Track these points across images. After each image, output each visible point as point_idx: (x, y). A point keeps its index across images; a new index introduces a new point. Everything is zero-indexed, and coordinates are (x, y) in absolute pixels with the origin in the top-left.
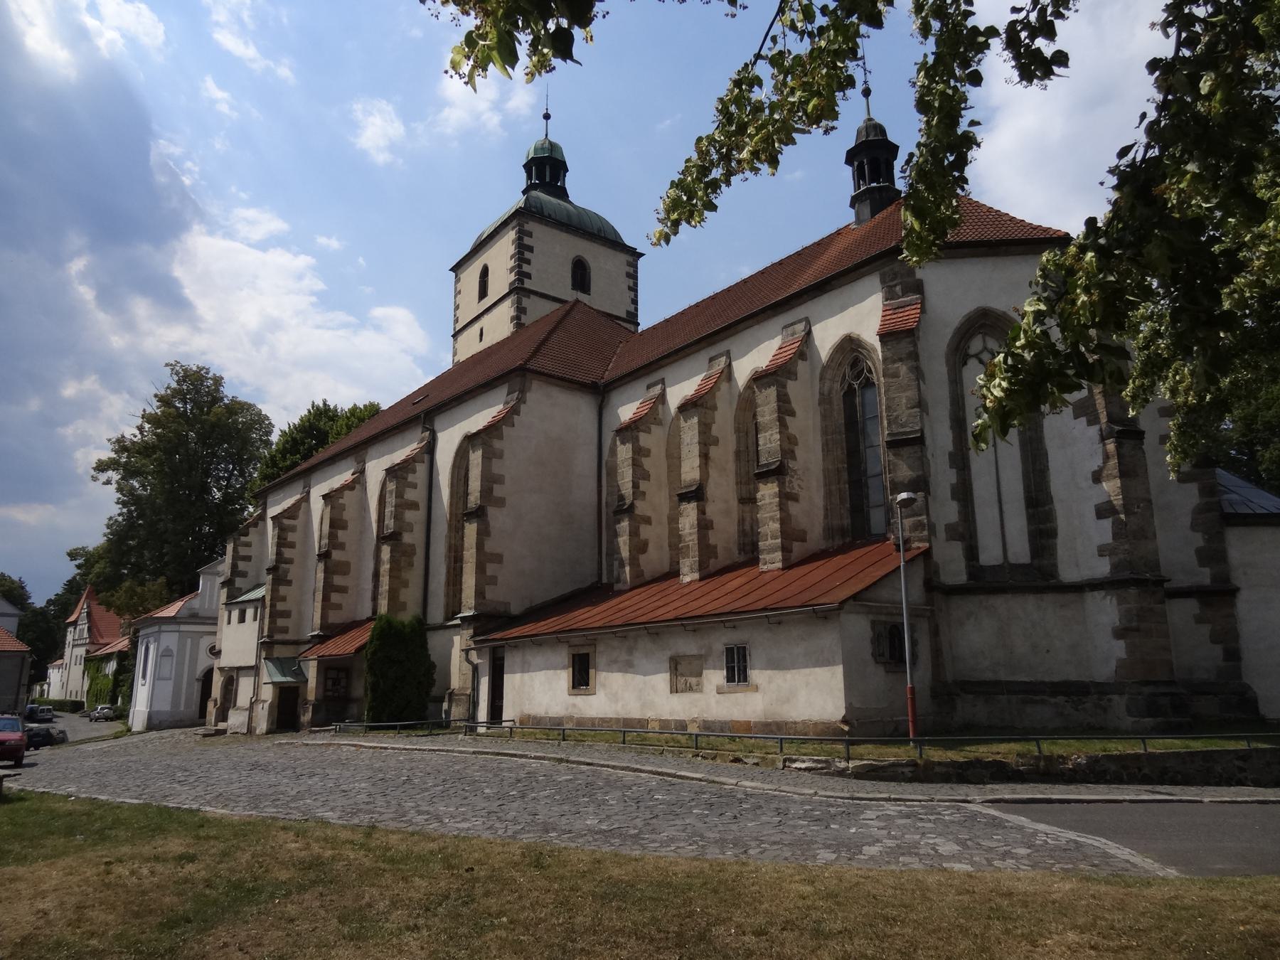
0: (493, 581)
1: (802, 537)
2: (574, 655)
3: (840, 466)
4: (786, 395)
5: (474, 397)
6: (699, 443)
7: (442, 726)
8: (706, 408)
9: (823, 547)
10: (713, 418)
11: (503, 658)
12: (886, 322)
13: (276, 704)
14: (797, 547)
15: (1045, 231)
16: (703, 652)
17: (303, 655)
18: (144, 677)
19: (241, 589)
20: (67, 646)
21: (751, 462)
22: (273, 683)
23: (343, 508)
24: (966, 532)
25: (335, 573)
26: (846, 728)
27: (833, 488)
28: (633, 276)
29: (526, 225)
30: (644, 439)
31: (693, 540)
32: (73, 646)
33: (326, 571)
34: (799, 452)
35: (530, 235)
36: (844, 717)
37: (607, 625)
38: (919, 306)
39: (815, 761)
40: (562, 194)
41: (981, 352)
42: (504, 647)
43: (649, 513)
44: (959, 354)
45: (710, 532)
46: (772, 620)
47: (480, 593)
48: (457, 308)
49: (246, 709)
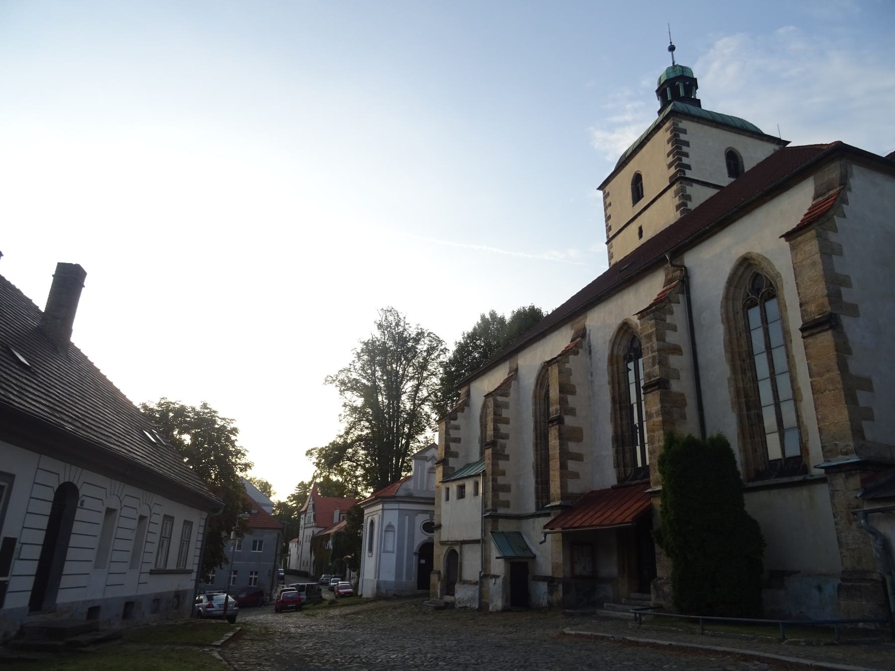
18: (371, 550)
19: (454, 468)
20: (300, 529)
23: (569, 373)
32: (304, 528)
33: (561, 437)
35: (684, 131)
40: (698, 103)
49: (476, 583)
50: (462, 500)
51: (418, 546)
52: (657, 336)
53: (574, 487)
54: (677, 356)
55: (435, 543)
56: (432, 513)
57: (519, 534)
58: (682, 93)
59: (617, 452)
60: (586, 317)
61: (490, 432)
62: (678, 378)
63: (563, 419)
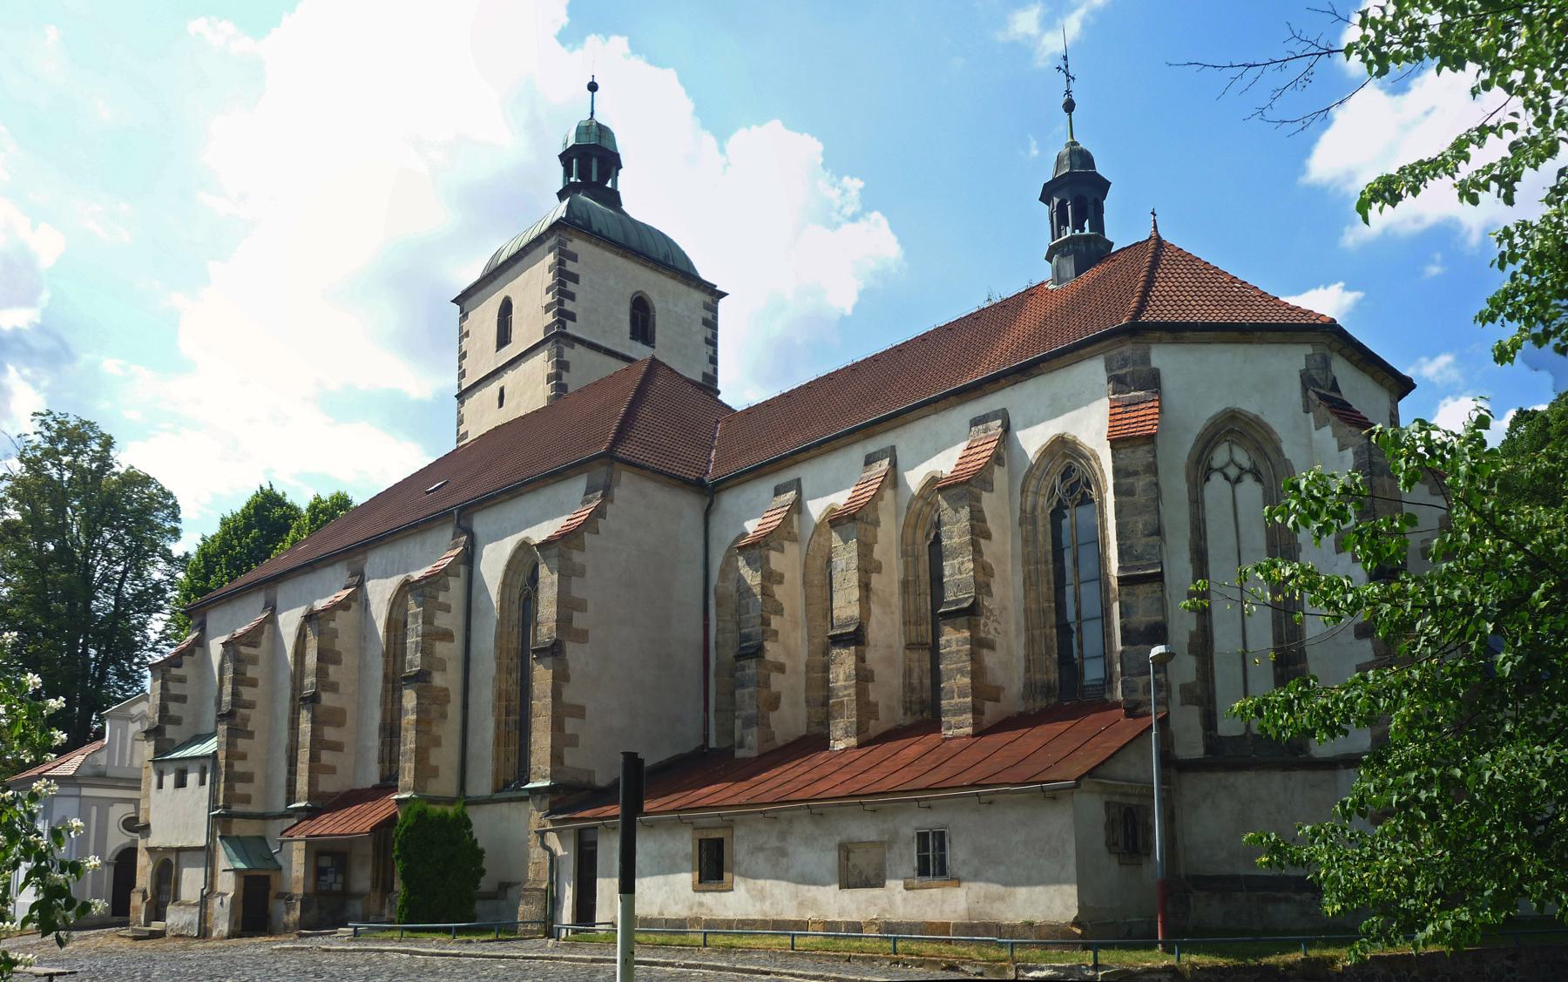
0: (573, 741)
1: (995, 694)
2: (700, 840)
3: (1046, 605)
4: (981, 511)
5: (534, 490)
6: (859, 569)
7: (507, 929)
8: (867, 523)
9: (1022, 710)
10: (875, 537)
11: (595, 844)
12: (1116, 424)
13: (241, 898)
14: (989, 706)
15: (1305, 314)
16: (886, 838)
17: (288, 833)
19: (173, 741)
21: (923, 596)
22: (236, 870)
24: (1204, 697)
25: (326, 723)
26: (1079, 931)
27: (1037, 632)
28: (711, 324)
29: (569, 243)
30: (776, 561)
31: (849, 695)
33: (314, 721)
34: (995, 588)
35: (574, 258)
36: (1076, 918)
37: (749, 802)
38: (1157, 404)
39: (1055, 969)
40: (613, 199)
41: (1227, 465)
42: (597, 828)
43: (782, 659)
44: (1201, 468)
45: (870, 686)
46: (983, 799)
47: (557, 757)
48: (463, 356)
49: (195, 905)
50: (181, 790)
51: (113, 852)
52: (423, 618)
53: (328, 785)
54: (446, 643)
55: (139, 848)
56: (136, 802)
57: (262, 839)
58: (594, 178)
59: (383, 744)
60: (366, 558)
61: (227, 698)
62: (444, 670)
63: (320, 696)
